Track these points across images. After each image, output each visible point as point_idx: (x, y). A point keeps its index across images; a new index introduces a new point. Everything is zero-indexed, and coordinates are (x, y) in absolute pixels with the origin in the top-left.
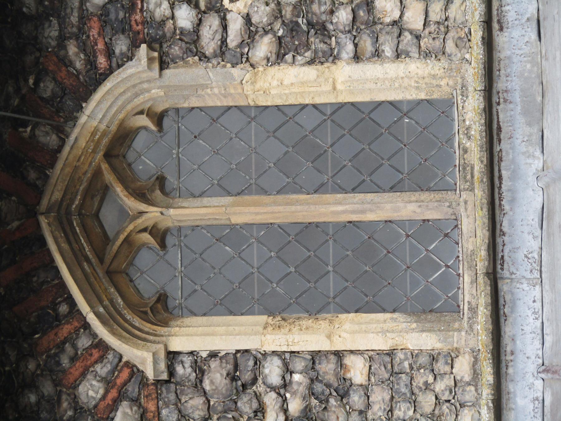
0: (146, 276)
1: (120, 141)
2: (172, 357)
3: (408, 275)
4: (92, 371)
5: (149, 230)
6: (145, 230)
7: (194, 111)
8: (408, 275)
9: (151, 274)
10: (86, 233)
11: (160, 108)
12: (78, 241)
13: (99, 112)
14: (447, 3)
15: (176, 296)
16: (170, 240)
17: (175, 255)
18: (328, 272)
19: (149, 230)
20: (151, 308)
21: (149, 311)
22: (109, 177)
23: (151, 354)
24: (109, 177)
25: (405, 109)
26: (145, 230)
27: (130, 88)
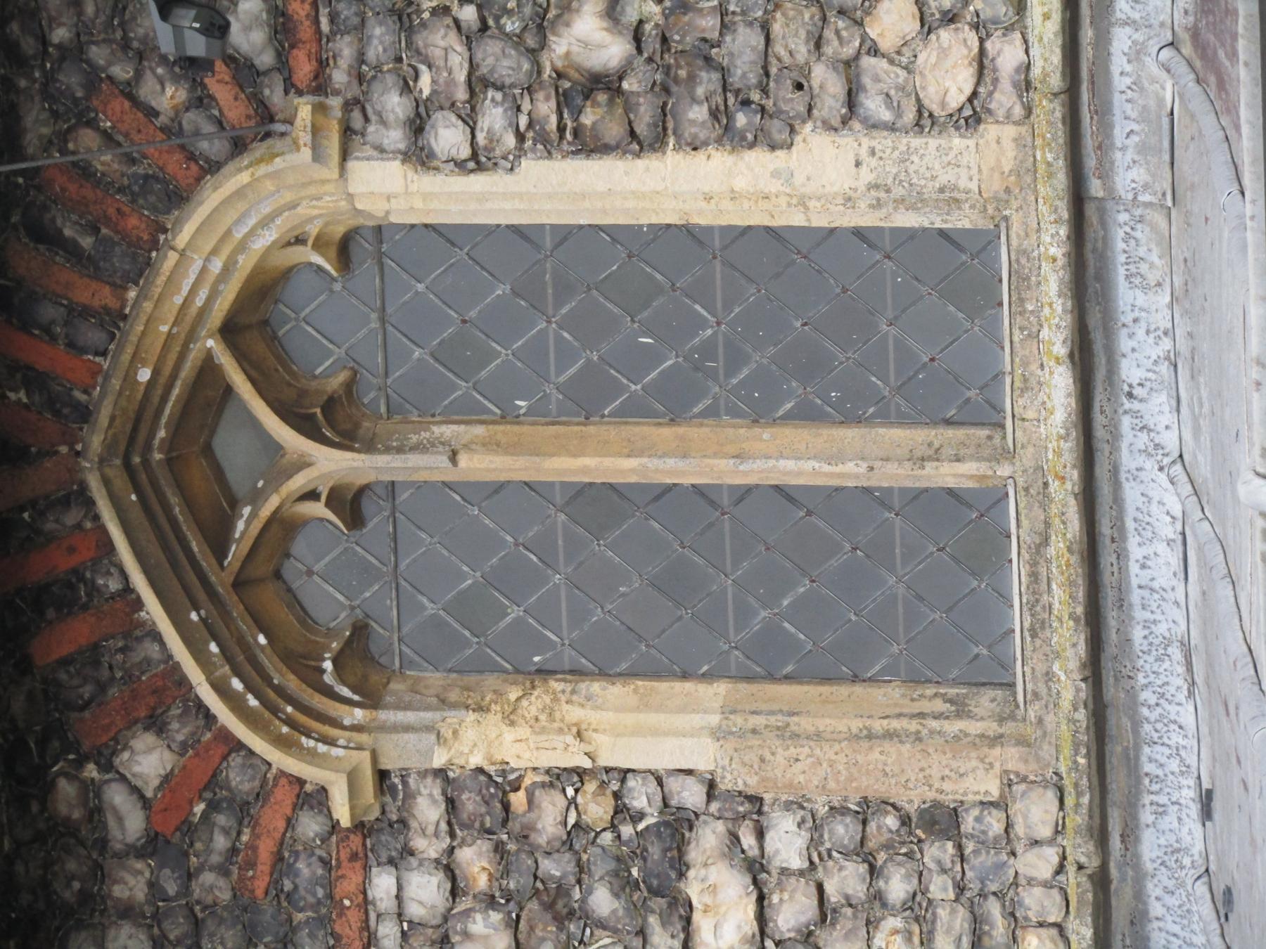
6: (312, 495)
17: (376, 520)
19: (310, 243)
26: (312, 495)
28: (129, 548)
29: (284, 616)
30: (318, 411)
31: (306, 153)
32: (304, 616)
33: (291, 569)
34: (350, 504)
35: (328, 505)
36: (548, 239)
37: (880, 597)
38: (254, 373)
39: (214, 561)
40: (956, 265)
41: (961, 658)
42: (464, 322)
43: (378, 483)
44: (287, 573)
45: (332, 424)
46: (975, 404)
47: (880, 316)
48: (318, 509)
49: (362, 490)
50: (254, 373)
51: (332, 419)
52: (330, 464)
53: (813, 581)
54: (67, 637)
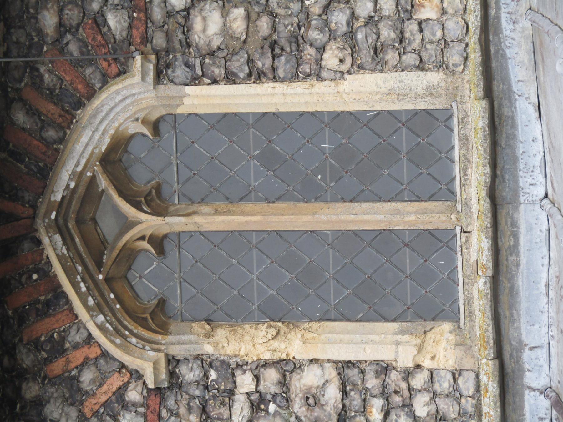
0: (144, 280)
1: (114, 159)
2: (173, 362)
3: (251, 133)
4: (94, 343)
5: (147, 239)
6: (142, 238)
7: (191, 116)
8: (251, 133)
9: (148, 280)
10: (81, 204)
11: (154, 116)
12: (73, 239)
13: (86, 143)
14: (330, 1)
15: (175, 304)
16: (168, 245)
17: (172, 253)
18: (328, 279)
19: (147, 239)
20: (150, 314)
21: (149, 318)
22: (103, 183)
23: (152, 364)
24: (103, 183)
25: (404, 119)
26: (142, 238)
27: (124, 103)
28: (63, 271)
29: (127, 295)
30: (143, 199)
31: (138, 78)
32: (137, 296)
33: (133, 275)
34: (159, 243)
35: (148, 242)
36: (251, 119)
37: (400, 281)
38: (110, 177)
39: (96, 268)
40: (428, 125)
41: (431, 306)
42: (212, 158)
43: (173, 233)
44: (129, 276)
45: (148, 205)
46: (443, 190)
47: (403, 151)
48: (145, 244)
49: (166, 236)
50: (115, 183)
51: (154, 201)
52: (149, 223)
53: (329, 245)
54: (42, 328)
